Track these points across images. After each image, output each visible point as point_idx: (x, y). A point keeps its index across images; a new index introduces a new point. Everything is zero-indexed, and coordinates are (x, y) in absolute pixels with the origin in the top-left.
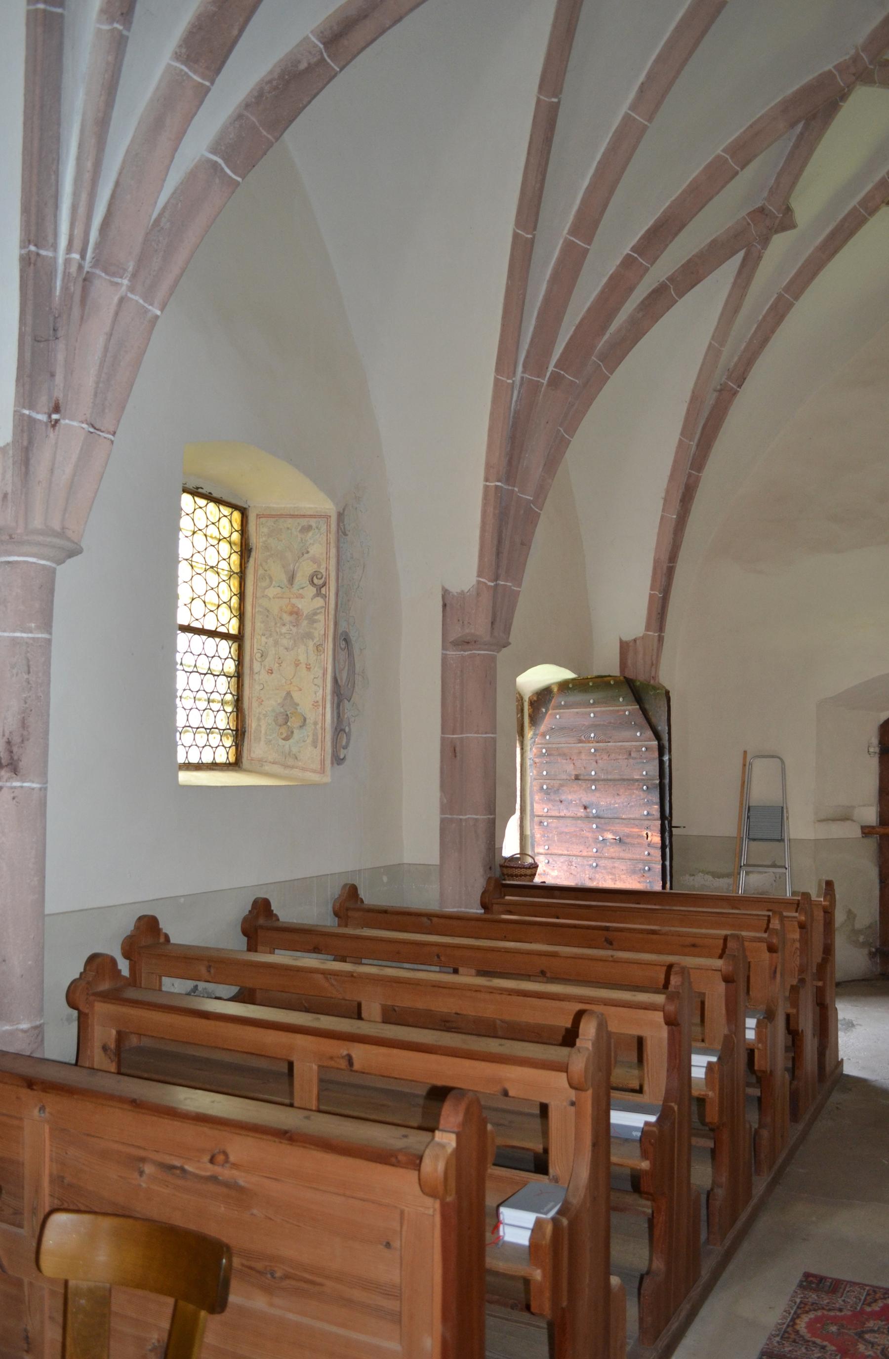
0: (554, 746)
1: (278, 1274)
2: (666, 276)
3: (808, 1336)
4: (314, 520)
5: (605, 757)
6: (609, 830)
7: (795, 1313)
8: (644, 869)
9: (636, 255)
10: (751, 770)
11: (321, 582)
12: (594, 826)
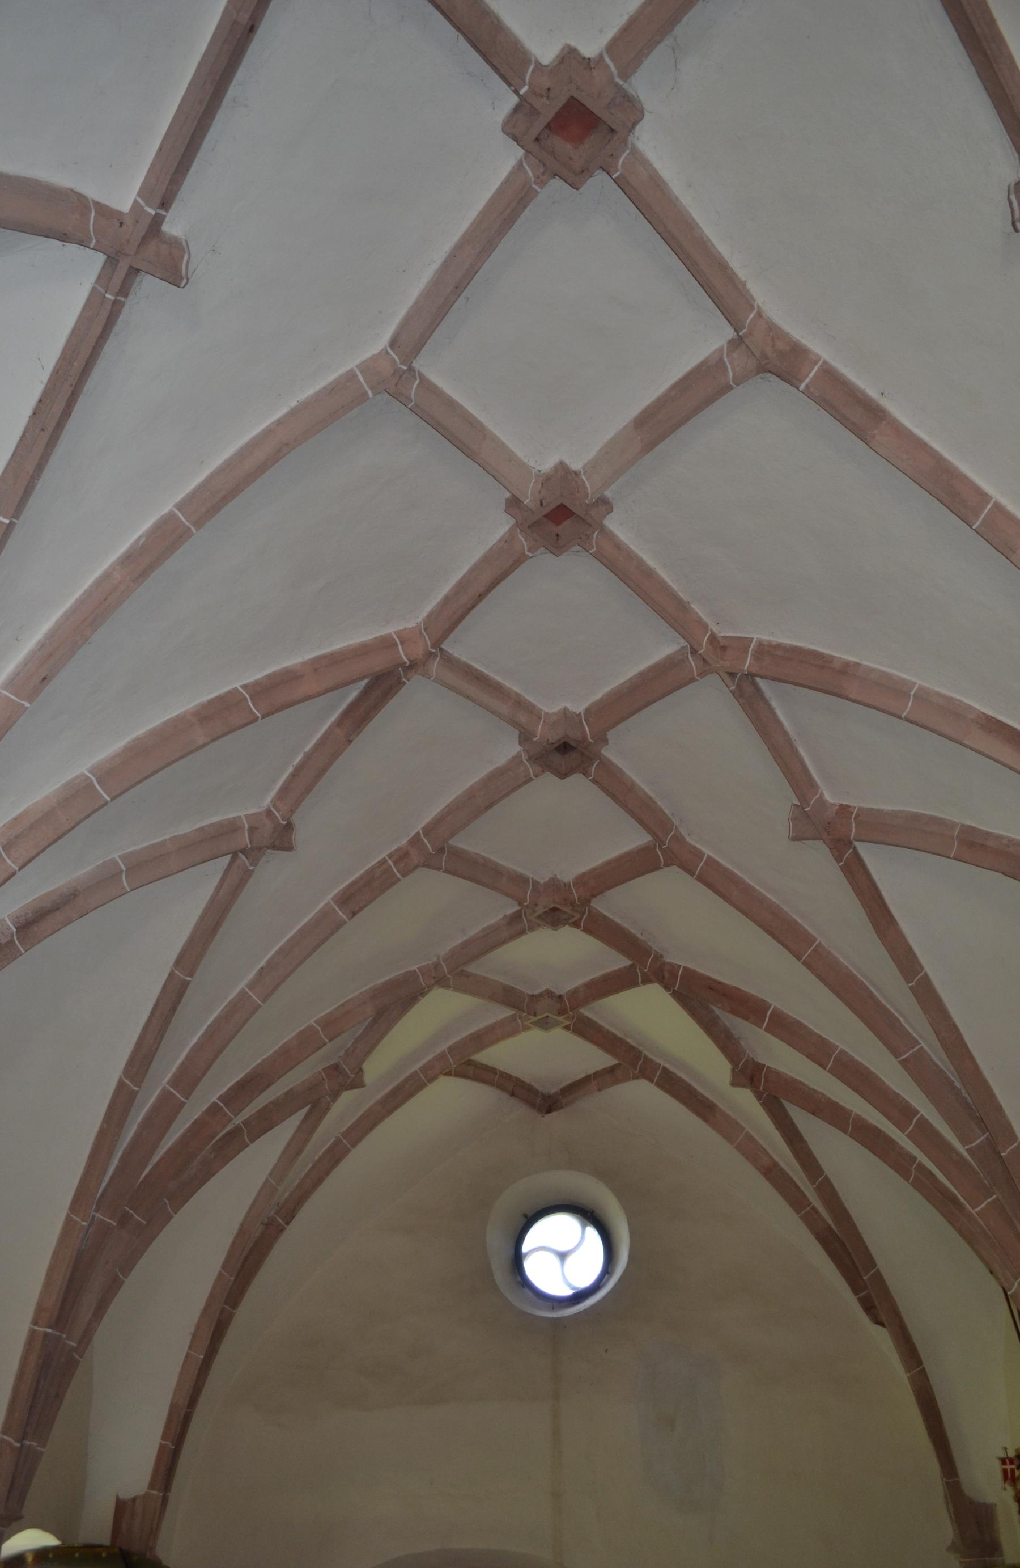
9: (222, 1105)
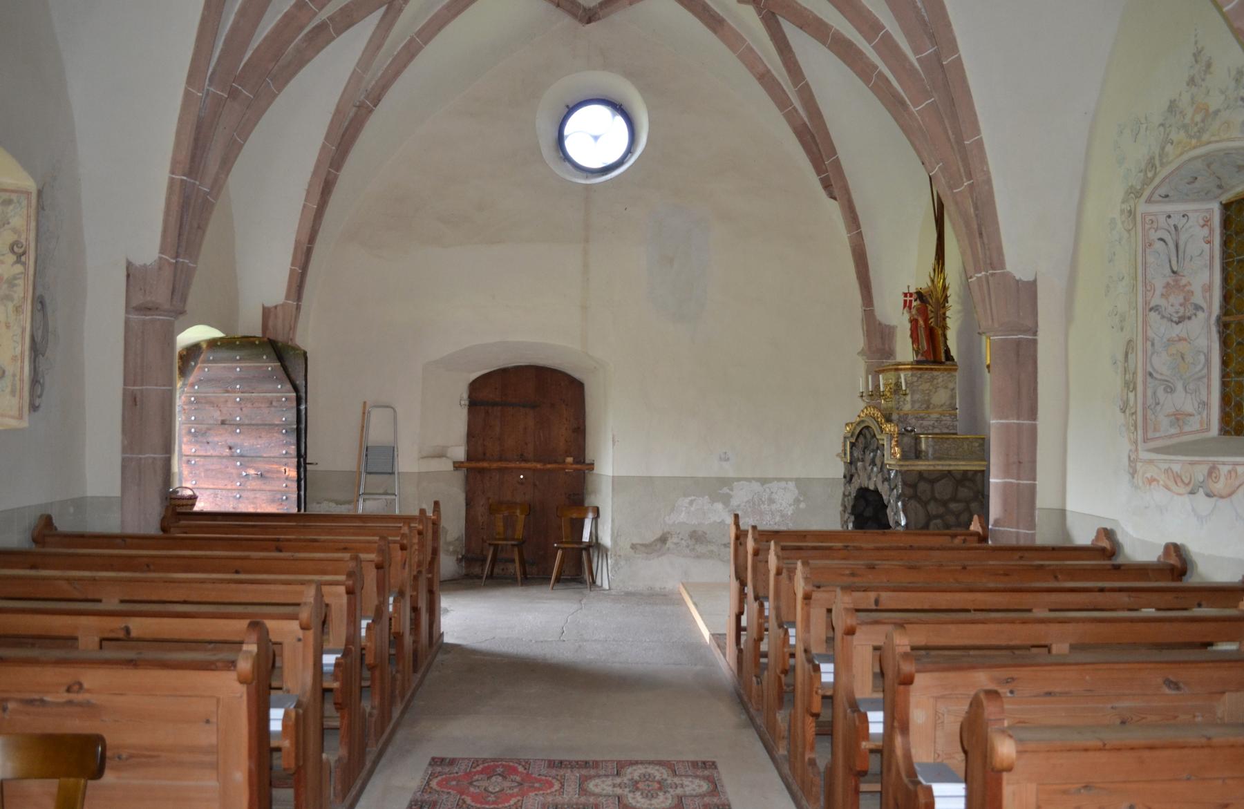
0: (203, 395)
1: (124, 756)
2: (327, 16)
3: (438, 789)
4: (16, 195)
5: (249, 405)
6: (251, 467)
7: (429, 778)
8: (282, 499)
10: (369, 417)
11: (21, 251)
12: (238, 463)
